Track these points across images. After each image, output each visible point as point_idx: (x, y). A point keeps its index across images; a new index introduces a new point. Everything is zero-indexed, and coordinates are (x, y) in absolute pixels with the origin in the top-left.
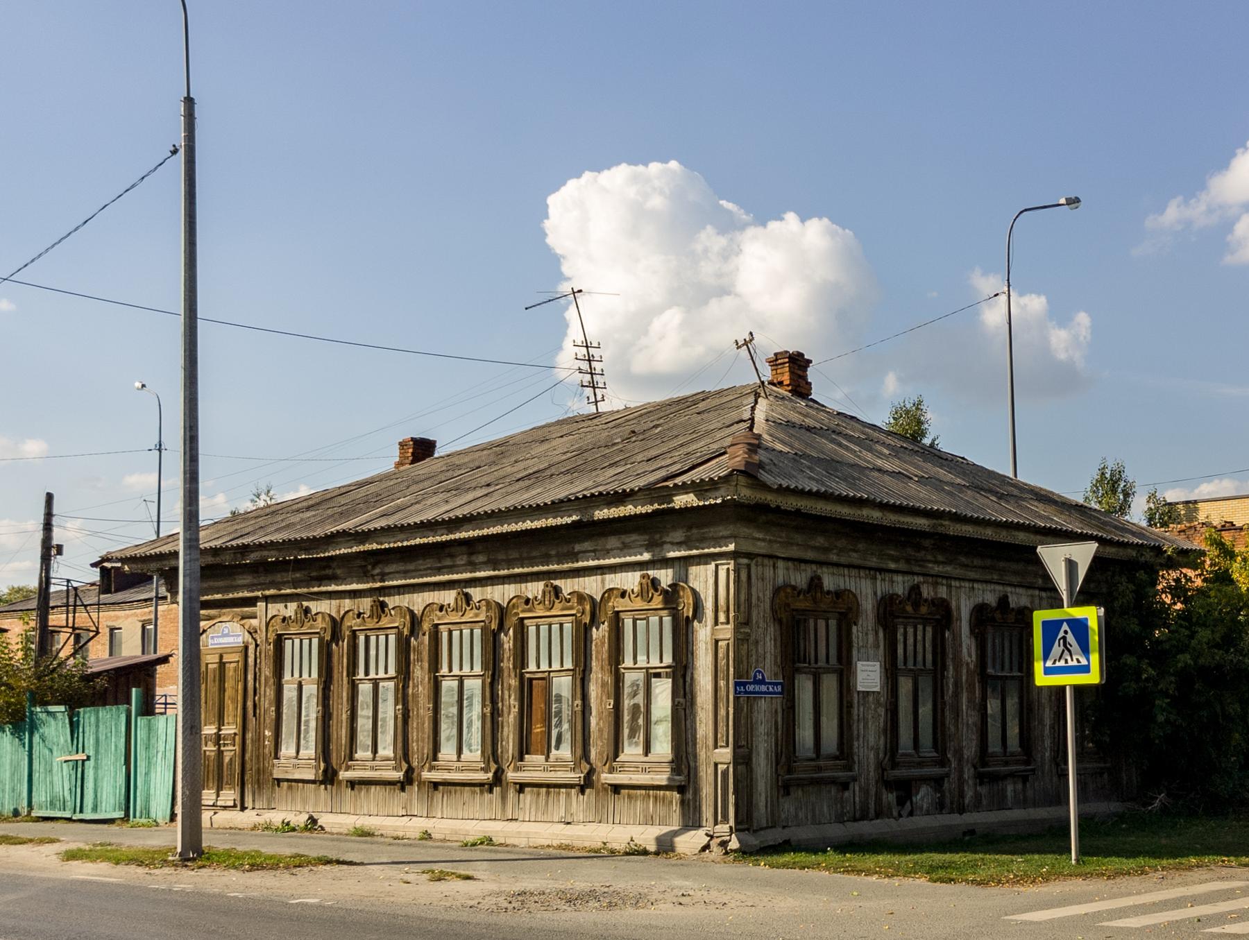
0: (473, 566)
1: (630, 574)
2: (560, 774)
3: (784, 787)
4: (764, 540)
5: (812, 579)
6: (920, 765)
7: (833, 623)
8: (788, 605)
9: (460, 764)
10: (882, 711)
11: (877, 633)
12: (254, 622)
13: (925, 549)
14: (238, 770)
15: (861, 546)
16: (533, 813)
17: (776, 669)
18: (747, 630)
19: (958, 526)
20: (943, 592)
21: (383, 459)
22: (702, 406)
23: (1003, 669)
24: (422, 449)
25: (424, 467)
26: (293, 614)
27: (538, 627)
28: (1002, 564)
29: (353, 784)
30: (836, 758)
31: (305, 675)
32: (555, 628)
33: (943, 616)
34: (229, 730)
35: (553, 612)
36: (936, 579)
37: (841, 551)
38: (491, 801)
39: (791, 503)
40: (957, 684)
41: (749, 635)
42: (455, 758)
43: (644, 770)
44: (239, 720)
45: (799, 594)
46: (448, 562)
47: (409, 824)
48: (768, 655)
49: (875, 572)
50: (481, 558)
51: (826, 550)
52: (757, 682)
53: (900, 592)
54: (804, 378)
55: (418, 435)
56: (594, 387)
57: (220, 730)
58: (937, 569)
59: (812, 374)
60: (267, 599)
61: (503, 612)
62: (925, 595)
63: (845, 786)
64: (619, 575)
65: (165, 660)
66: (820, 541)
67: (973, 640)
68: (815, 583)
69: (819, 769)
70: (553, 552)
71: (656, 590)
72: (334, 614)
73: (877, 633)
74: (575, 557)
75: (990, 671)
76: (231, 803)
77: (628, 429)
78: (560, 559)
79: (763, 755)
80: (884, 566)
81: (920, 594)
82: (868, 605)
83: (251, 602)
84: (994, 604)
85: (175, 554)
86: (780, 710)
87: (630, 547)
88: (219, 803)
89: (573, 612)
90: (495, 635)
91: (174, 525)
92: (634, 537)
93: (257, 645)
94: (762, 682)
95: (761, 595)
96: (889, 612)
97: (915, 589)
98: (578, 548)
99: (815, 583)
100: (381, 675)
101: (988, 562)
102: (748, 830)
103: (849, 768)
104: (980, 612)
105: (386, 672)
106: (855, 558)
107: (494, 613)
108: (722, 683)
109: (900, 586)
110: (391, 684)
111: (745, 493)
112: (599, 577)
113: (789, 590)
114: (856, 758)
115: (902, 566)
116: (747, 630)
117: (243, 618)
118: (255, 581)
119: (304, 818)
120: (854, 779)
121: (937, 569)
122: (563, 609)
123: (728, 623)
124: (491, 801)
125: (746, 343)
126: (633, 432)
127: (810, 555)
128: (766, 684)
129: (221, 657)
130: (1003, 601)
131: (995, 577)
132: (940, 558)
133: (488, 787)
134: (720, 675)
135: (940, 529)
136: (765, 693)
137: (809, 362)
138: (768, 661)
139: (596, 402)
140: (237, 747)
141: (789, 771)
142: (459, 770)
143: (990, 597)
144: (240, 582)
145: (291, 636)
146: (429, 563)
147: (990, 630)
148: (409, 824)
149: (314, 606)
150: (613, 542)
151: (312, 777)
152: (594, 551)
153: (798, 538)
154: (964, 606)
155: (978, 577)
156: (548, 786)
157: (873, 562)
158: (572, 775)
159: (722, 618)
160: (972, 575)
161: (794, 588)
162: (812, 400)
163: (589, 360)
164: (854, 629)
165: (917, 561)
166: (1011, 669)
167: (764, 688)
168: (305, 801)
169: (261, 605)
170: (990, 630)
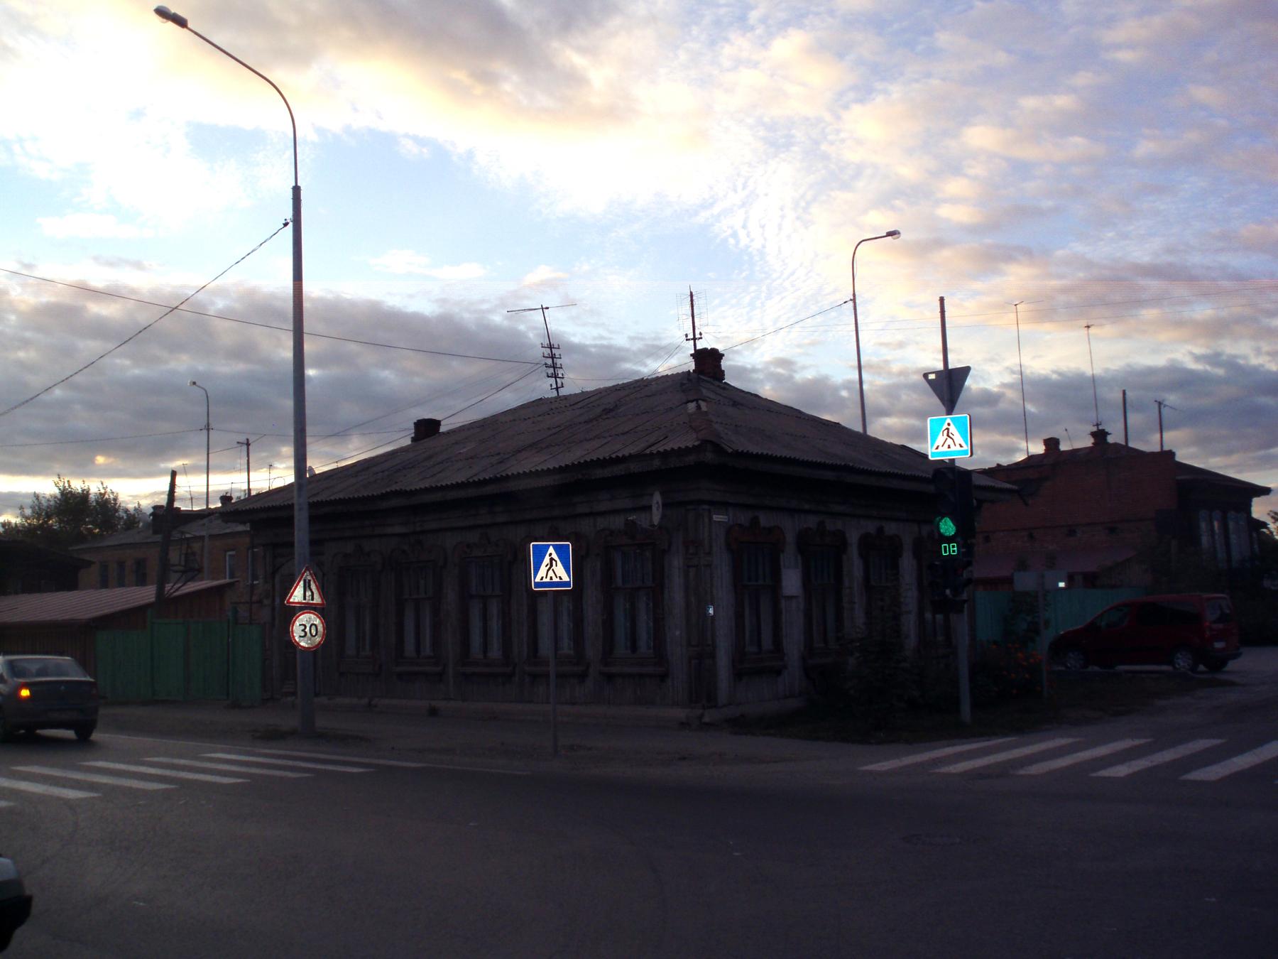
3: (739, 674)
25: (429, 443)
33: (841, 545)
63: (778, 672)
82: (790, 538)
99: (755, 521)
111: (709, 457)
119: (365, 701)
130: (880, 530)
161: (740, 525)
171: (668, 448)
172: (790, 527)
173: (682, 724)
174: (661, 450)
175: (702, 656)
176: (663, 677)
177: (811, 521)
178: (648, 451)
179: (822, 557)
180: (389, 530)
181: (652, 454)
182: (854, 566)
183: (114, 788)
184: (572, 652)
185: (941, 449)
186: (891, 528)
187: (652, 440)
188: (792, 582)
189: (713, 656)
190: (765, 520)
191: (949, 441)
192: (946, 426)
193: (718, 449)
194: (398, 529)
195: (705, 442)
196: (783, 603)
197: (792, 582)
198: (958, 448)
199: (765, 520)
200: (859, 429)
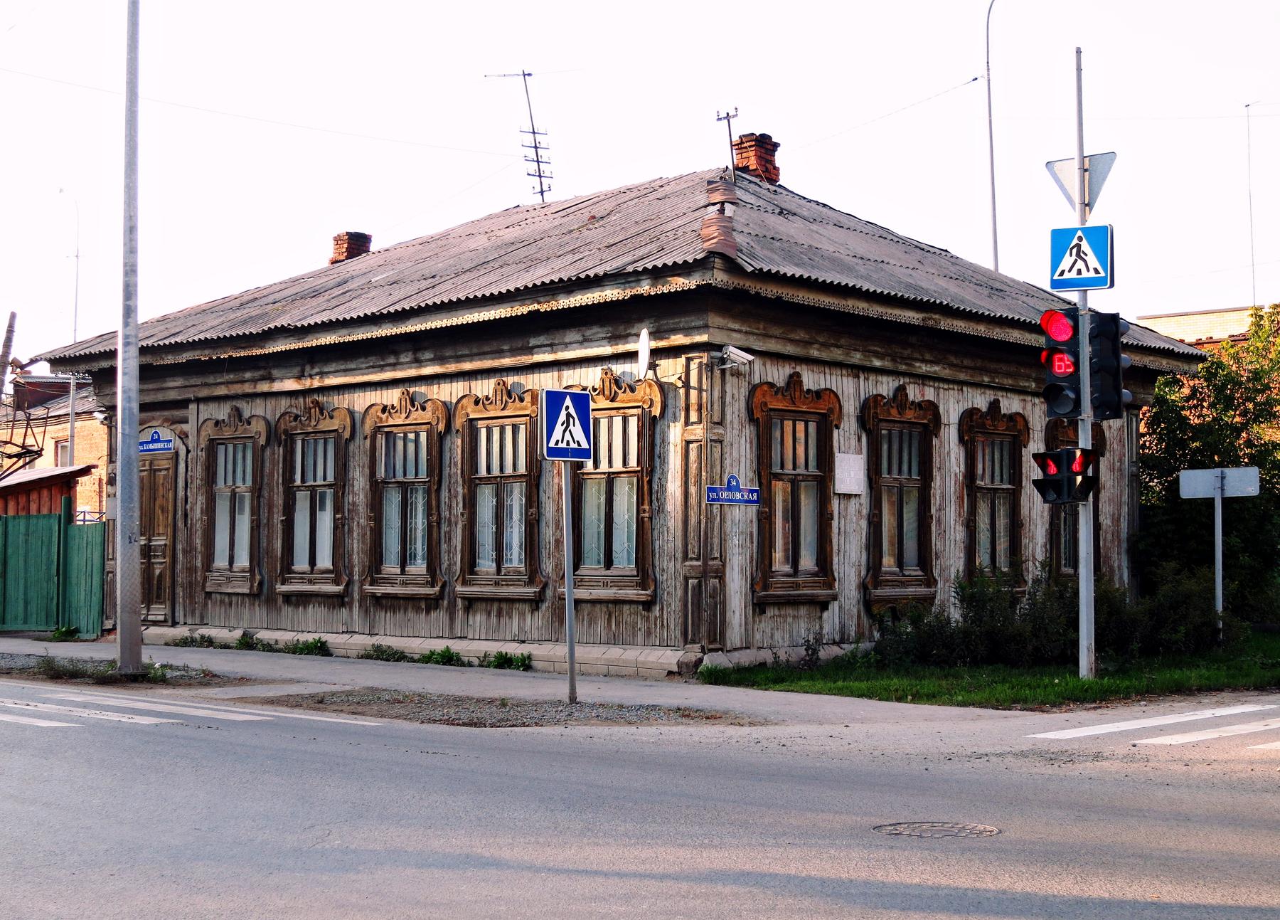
0: (418, 362)
1: (584, 370)
2: (512, 589)
3: (759, 606)
4: (739, 331)
5: (791, 376)
6: (903, 584)
7: (812, 427)
8: (766, 404)
9: (404, 578)
10: (864, 524)
11: (859, 439)
12: (185, 427)
13: (912, 346)
14: (168, 582)
15: (843, 341)
16: (483, 630)
17: (751, 475)
18: (721, 431)
19: (949, 321)
20: (930, 394)
21: (317, 255)
22: (660, 194)
23: (992, 481)
24: (356, 244)
25: (358, 264)
26: (226, 418)
27: (489, 430)
28: (993, 366)
29: (288, 598)
30: (815, 574)
31: (239, 483)
32: (509, 431)
33: (931, 417)
34: (159, 541)
35: (506, 413)
36: (924, 379)
37: (824, 345)
38: (437, 620)
39: (770, 291)
40: (943, 497)
41: (723, 435)
42: (398, 571)
43: (606, 585)
44: (169, 531)
45: (776, 393)
46: (392, 360)
47: (351, 641)
48: (743, 459)
49: (856, 370)
50: (428, 355)
51: (807, 344)
52: (729, 488)
53: (885, 394)
54: (772, 162)
55: (352, 230)
56: (540, 176)
57: (150, 540)
58: (924, 368)
59: (780, 159)
60: (198, 400)
61: (449, 411)
62: (911, 397)
63: (824, 606)
64: (578, 371)
65: (86, 471)
66: (801, 335)
67: (962, 449)
68: (795, 380)
69: (797, 586)
70: (506, 348)
71: (620, 388)
72: (269, 417)
73: (859, 439)
74: (530, 350)
75: (980, 483)
76: (161, 618)
77: (587, 215)
78: (514, 352)
79: (737, 569)
80: (868, 364)
81: (906, 395)
82: (850, 408)
83: (183, 404)
84: (984, 409)
85: (112, 354)
86: (755, 520)
87: (591, 341)
88: (150, 618)
89: (527, 412)
90: (441, 437)
91: (113, 322)
92: (595, 329)
93: (188, 451)
94: (738, 489)
95: (735, 392)
96: (869, 414)
97: (901, 390)
98: (533, 342)
99: (795, 380)
100: (320, 482)
101: (979, 363)
102: (722, 650)
103: (831, 586)
104: (970, 420)
105: (325, 479)
106: (837, 354)
107: (441, 413)
108: (693, 490)
109: (886, 386)
110: (329, 492)
111: (718, 277)
112: (556, 374)
113: (765, 388)
114: (836, 575)
115: (887, 364)
116: (721, 431)
117: (173, 423)
118: (187, 383)
119: (238, 634)
120: (835, 598)
121: (924, 368)
122: (516, 409)
123: (700, 422)
124: (437, 620)
125: (728, 117)
126: (594, 217)
127: (790, 349)
128: (740, 491)
129: (151, 464)
130: (994, 405)
131: (986, 379)
132: (928, 357)
133: (432, 604)
134: (692, 480)
135: (930, 323)
136: (739, 501)
137: (776, 145)
138: (742, 465)
139: (542, 192)
140: (167, 560)
141: (765, 588)
142: (404, 584)
143: (981, 401)
144: (171, 384)
145: (223, 442)
146: (372, 361)
147: (980, 438)
148: (351, 641)
149: (247, 409)
150: (572, 336)
151: (246, 591)
152: (551, 345)
153: (777, 331)
154: (953, 406)
155: (967, 378)
156: (500, 600)
157: (857, 358)
158: (526, 590)
159: (693, 417)
160: (962, 377)
161: (772, 385)
162: (780, 186)
163: (536, 147)
164: (836, 432)
165: (902, 358)
166: (1002, 481)
167: (738, 496)
168: (239, 618)
169: (193, 407)
170: (980, 438)
171: (659, 264)
172: (850, 392)
173: (670, 673)
174: (650, 266)
175: (710, 572)
176: (648, 605)
177: (886, 386)
178: (630, 269)
179: (900, 437)
180: (278, 386)
181: (635, 272)
182: (950, 454)
183: (118, 726)
184: (522, 567)
185: (1067, 276)
186: (1011, 404)
187: (640, 253)
188: (850, 472)
189: (720, 575)
190: (812, 380)
191: (1080, 264)
192: (1075, 241)
193: (732, 266)
194: (290, 385)
195: (711, 254)
196: (835, 505)
197: (850, 472)
198: (1092, 274)
199: (812, 380)
200: (988, 264)
